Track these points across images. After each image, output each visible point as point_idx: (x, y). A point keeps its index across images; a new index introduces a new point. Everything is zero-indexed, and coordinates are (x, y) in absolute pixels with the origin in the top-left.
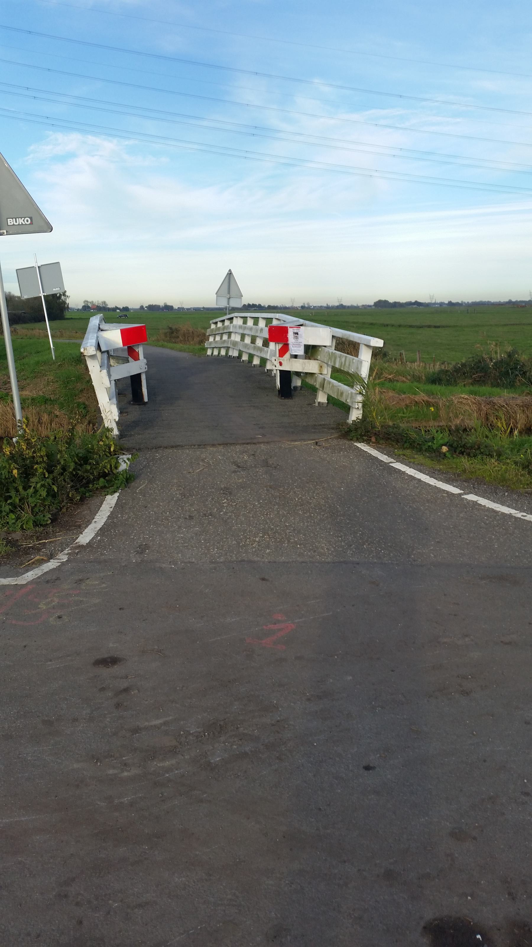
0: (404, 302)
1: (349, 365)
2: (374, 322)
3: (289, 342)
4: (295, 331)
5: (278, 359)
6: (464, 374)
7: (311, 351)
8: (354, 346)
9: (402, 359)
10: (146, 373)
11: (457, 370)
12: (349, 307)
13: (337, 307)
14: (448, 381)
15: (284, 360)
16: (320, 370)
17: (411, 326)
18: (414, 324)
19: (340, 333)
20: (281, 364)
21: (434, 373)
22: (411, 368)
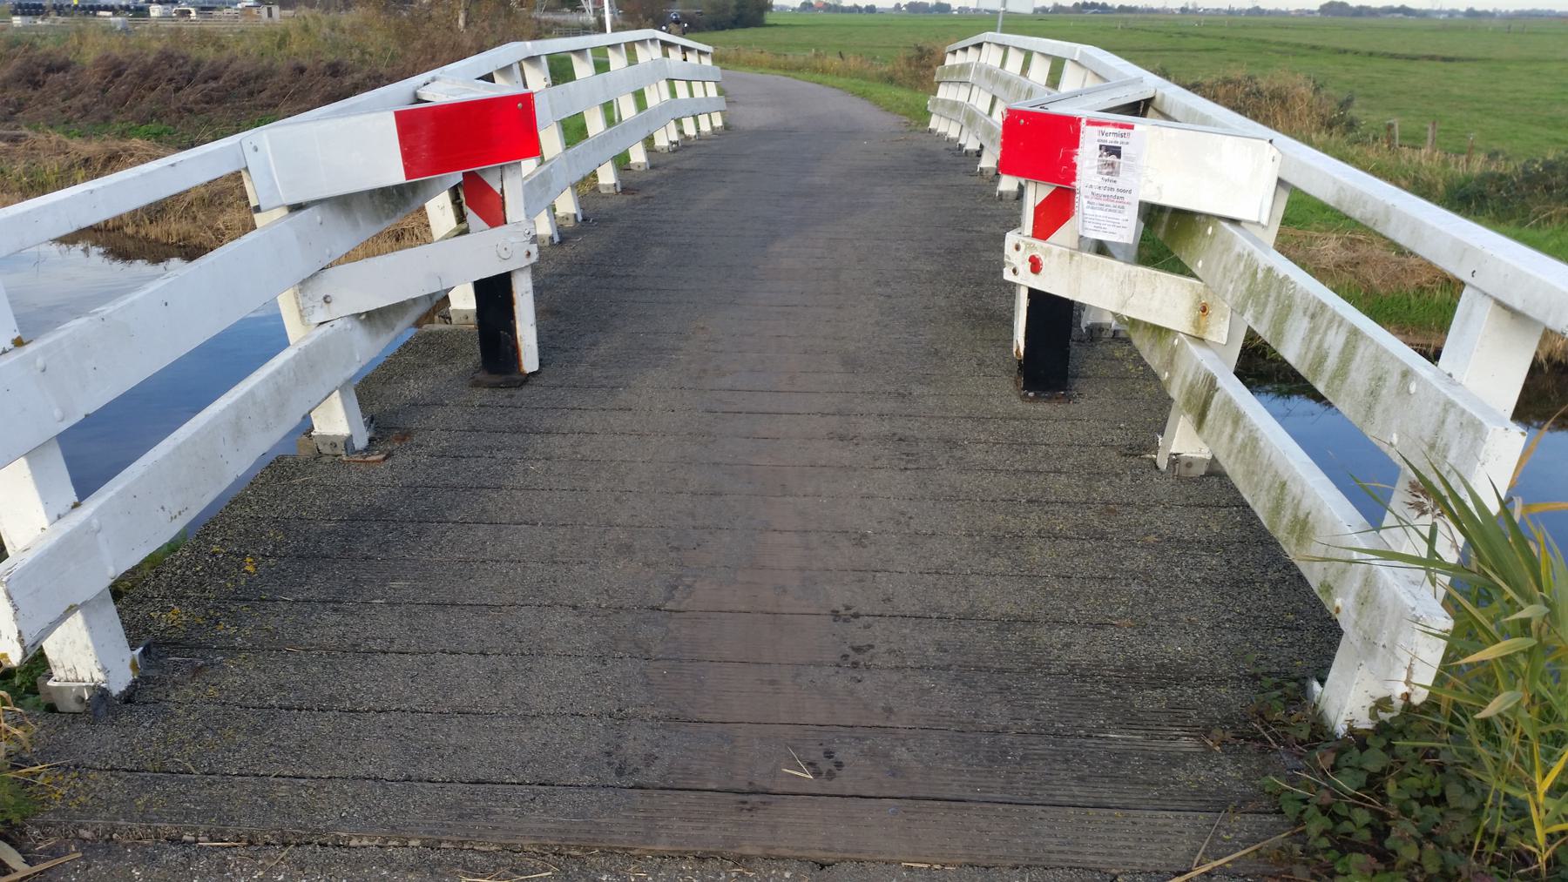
0: (1379, 6)
1: (1373, 393)
2: (1320, 43)
3: (1077, 184)
4: (1111, 141)
5: (1029, 246)
6: (1549, 189)
7: (1166, 236)
8: (1284, 102)
9: (1390, 138)
10: (534, 269)
11: (1531, 179)
12: (1270, 13)
13: (1249, 12)
14: (1505, 202)
15: (1048, 252)
16: (1196, 324)
17: (1393, 56)
18: (1400, 52)
19: (1330, 176)
20: (1036, 266)
21: (1468, 180)
22: (1410, 161)
